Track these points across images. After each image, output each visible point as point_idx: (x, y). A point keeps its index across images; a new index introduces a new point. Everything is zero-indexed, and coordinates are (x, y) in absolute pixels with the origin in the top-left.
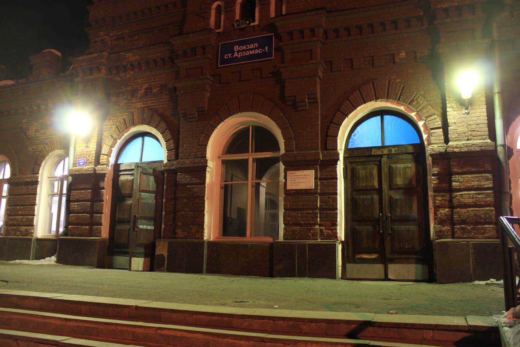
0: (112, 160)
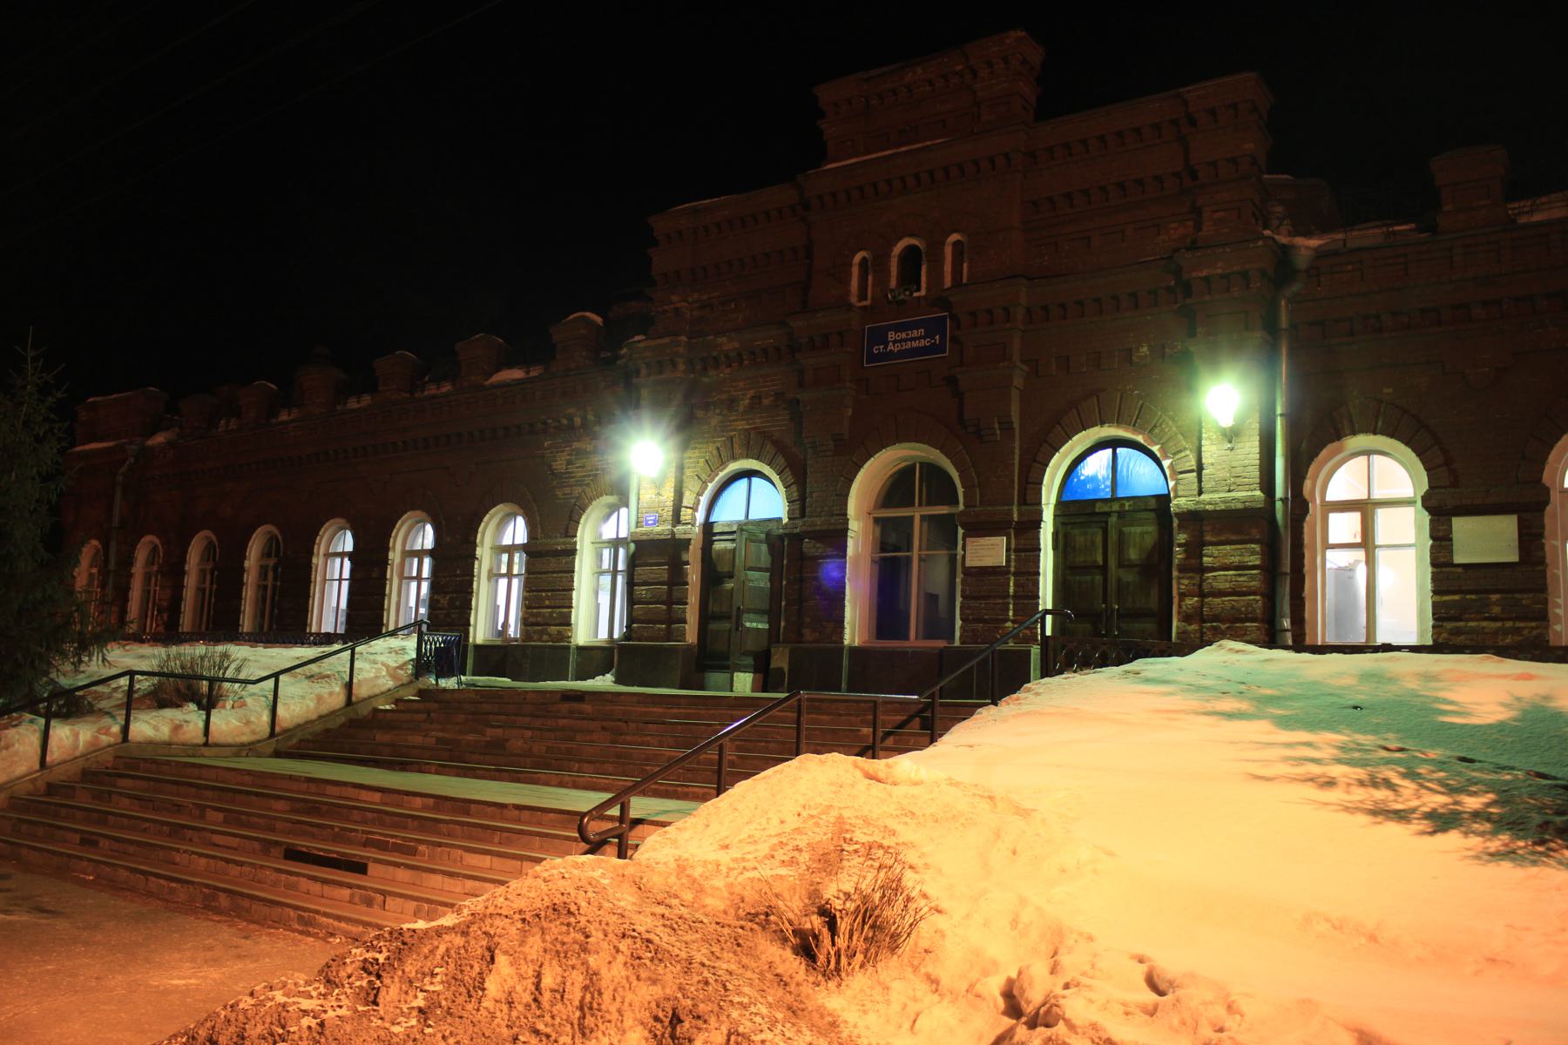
0: (700, 516)
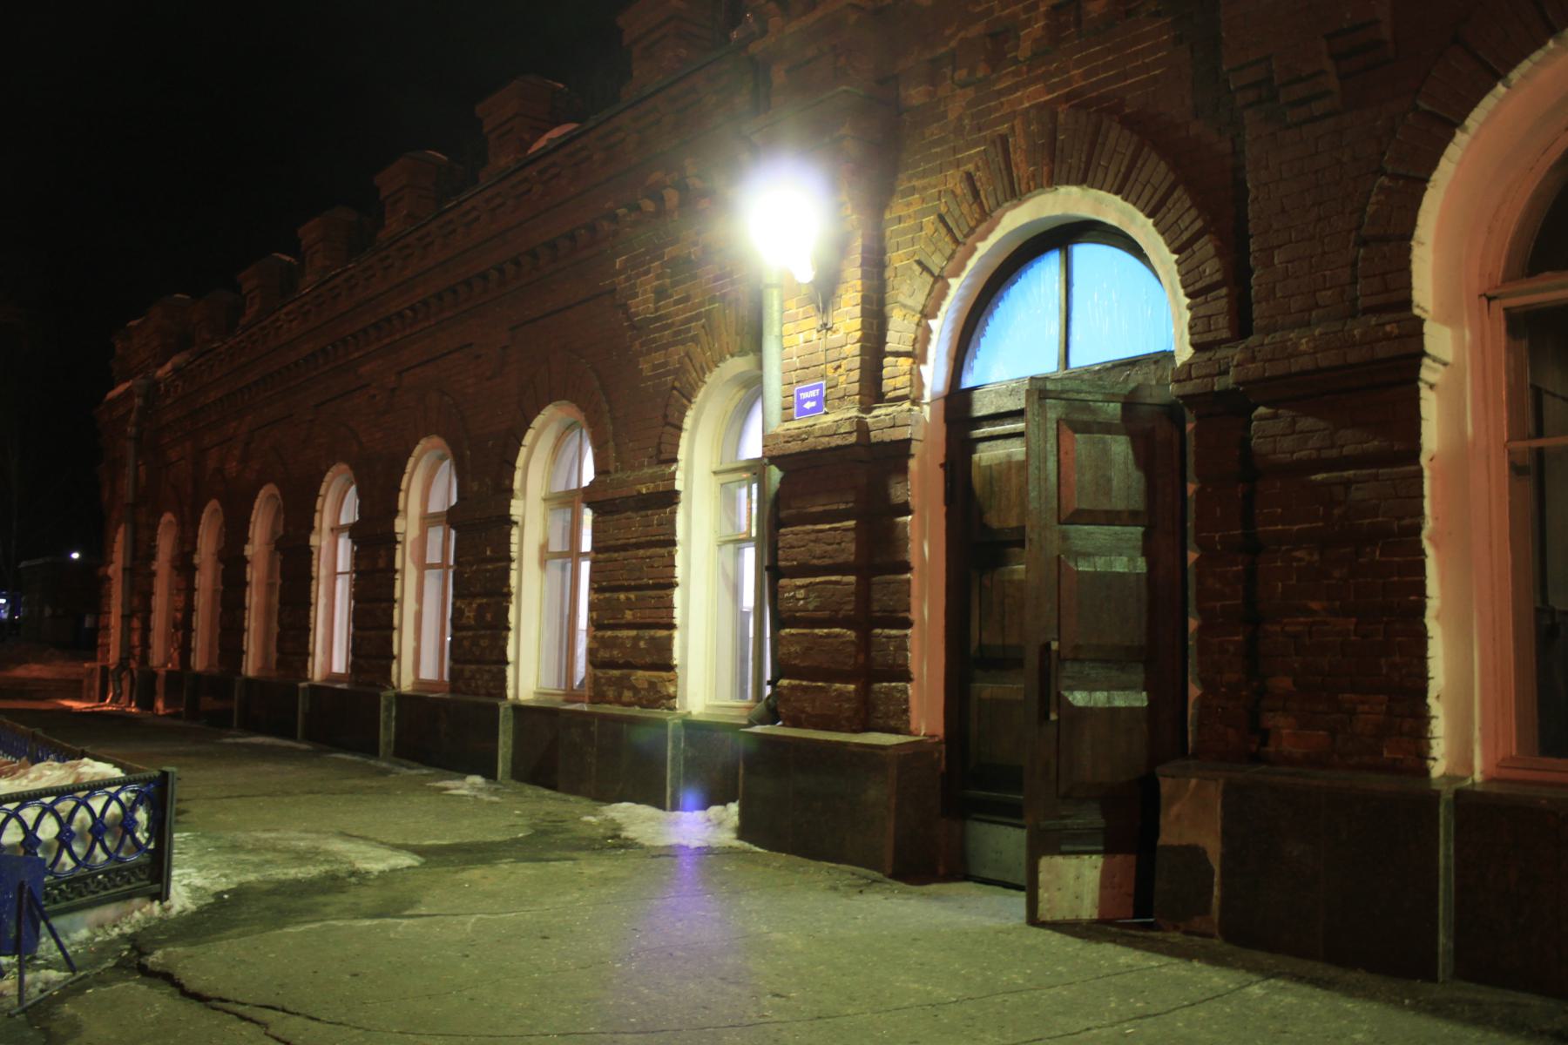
0: (934, 376)
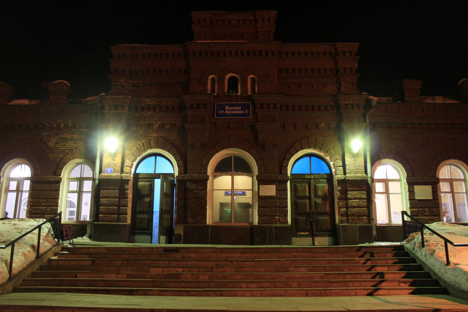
0: (133, 170)
